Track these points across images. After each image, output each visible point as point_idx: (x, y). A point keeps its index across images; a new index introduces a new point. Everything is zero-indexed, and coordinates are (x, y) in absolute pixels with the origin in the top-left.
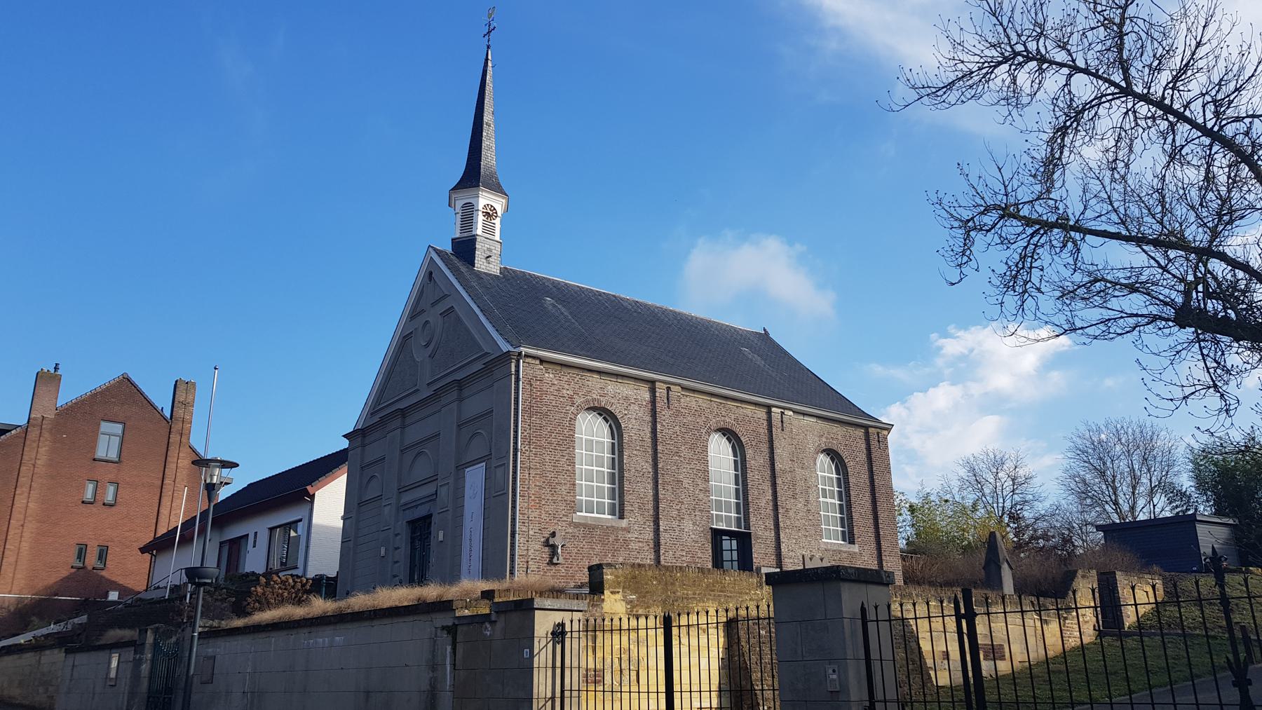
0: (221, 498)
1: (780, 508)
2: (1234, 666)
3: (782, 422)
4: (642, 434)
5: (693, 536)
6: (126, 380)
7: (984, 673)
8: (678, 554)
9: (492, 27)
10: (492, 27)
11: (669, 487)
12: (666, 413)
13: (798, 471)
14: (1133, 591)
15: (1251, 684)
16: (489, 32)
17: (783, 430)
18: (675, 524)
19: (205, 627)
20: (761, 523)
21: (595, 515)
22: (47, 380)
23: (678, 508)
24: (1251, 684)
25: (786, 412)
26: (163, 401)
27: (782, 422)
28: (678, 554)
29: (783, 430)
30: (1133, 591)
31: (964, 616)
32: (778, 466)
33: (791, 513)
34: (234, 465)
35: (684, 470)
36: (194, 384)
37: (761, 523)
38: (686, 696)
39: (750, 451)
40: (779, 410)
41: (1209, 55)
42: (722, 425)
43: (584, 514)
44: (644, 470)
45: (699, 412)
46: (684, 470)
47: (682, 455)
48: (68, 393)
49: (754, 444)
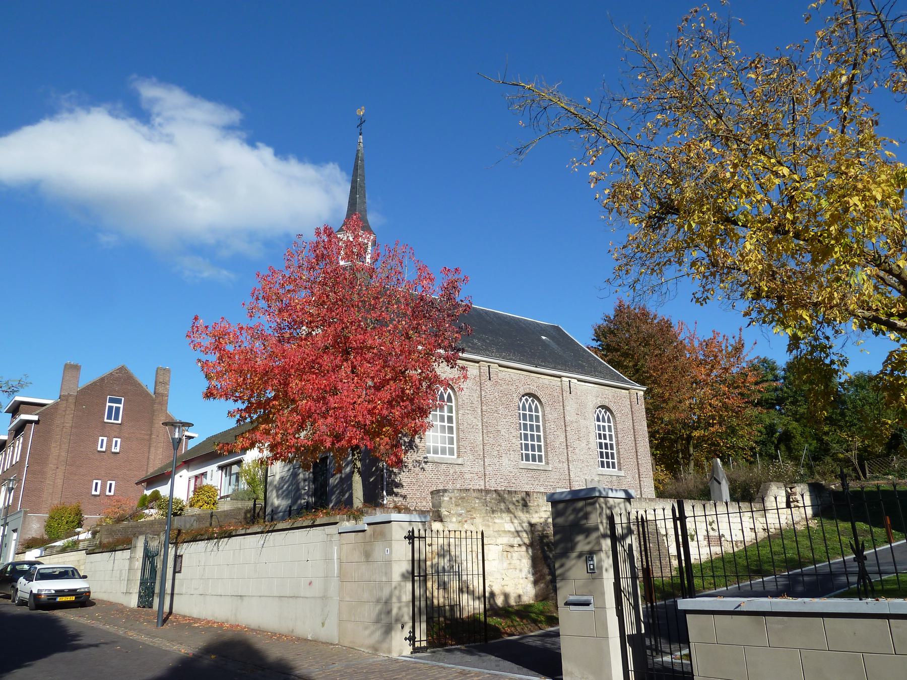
0: (189, 448)
1: (569, 447)
2: (855, 547)
3: (570, 387)
4: (472, 399)
5: (509, 469)
6: (122, 369)
7: (693, 561)
8: (498, 482)
9: (363, 120)
10: (363, 120)
11: (491, 435)
12: (488, 383)
13: (582, 421)
14: (803, 498)
15: (866, 560)
16: (361, 124)
17: (570, 393)
18: (496, 460)
19: (504, 628)
20: (556, 458)
21: (440, 455)
22: (72, 369)
23: (498, 449)
24: (866, 560)
25: (573, 380)
26: (147, 382)
27: (570, 387)
28: (498, 482)
29: (570, 393)
30: (803, 498)
31: (678, 519)
32: (568, 418)
33: (577, 451)
34: (189, 425)
35: (502, 423)
36: (169, 371)
37: (556, 458)
38: (475, 572)
39: (548, 409)
40: (568, 379)
41: (538, 117)
42: (528, 391)
43: (440, 455)
44: (474, 424)
45: (511, 382)
46: (502, 423)
47: (500, 412)
48: (86, 379)
49: (550, 403)
